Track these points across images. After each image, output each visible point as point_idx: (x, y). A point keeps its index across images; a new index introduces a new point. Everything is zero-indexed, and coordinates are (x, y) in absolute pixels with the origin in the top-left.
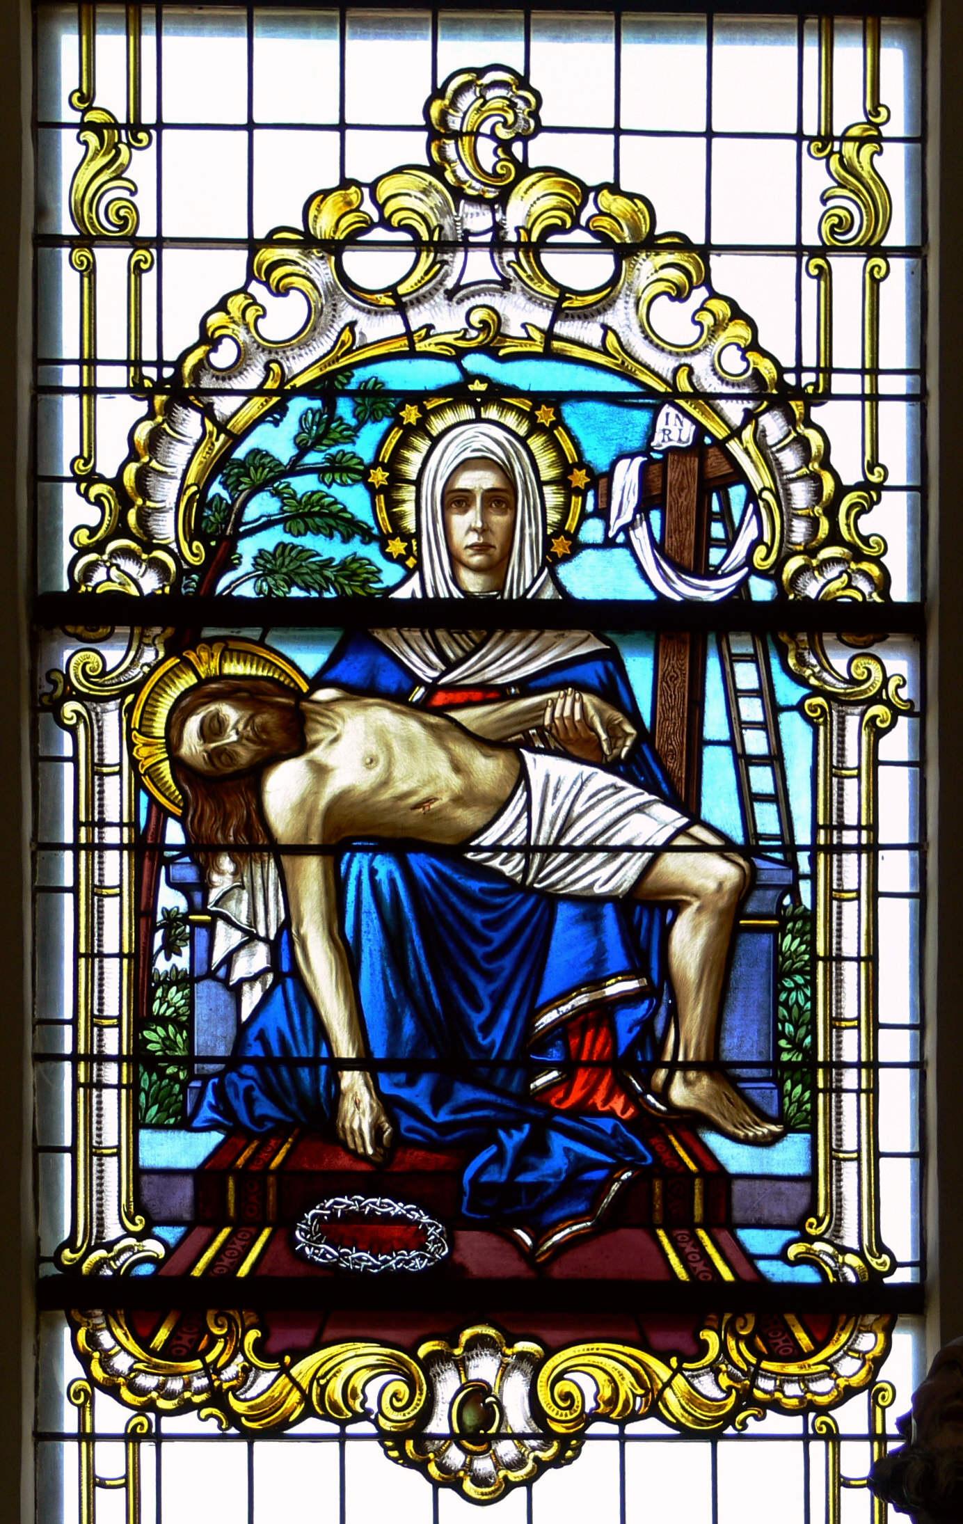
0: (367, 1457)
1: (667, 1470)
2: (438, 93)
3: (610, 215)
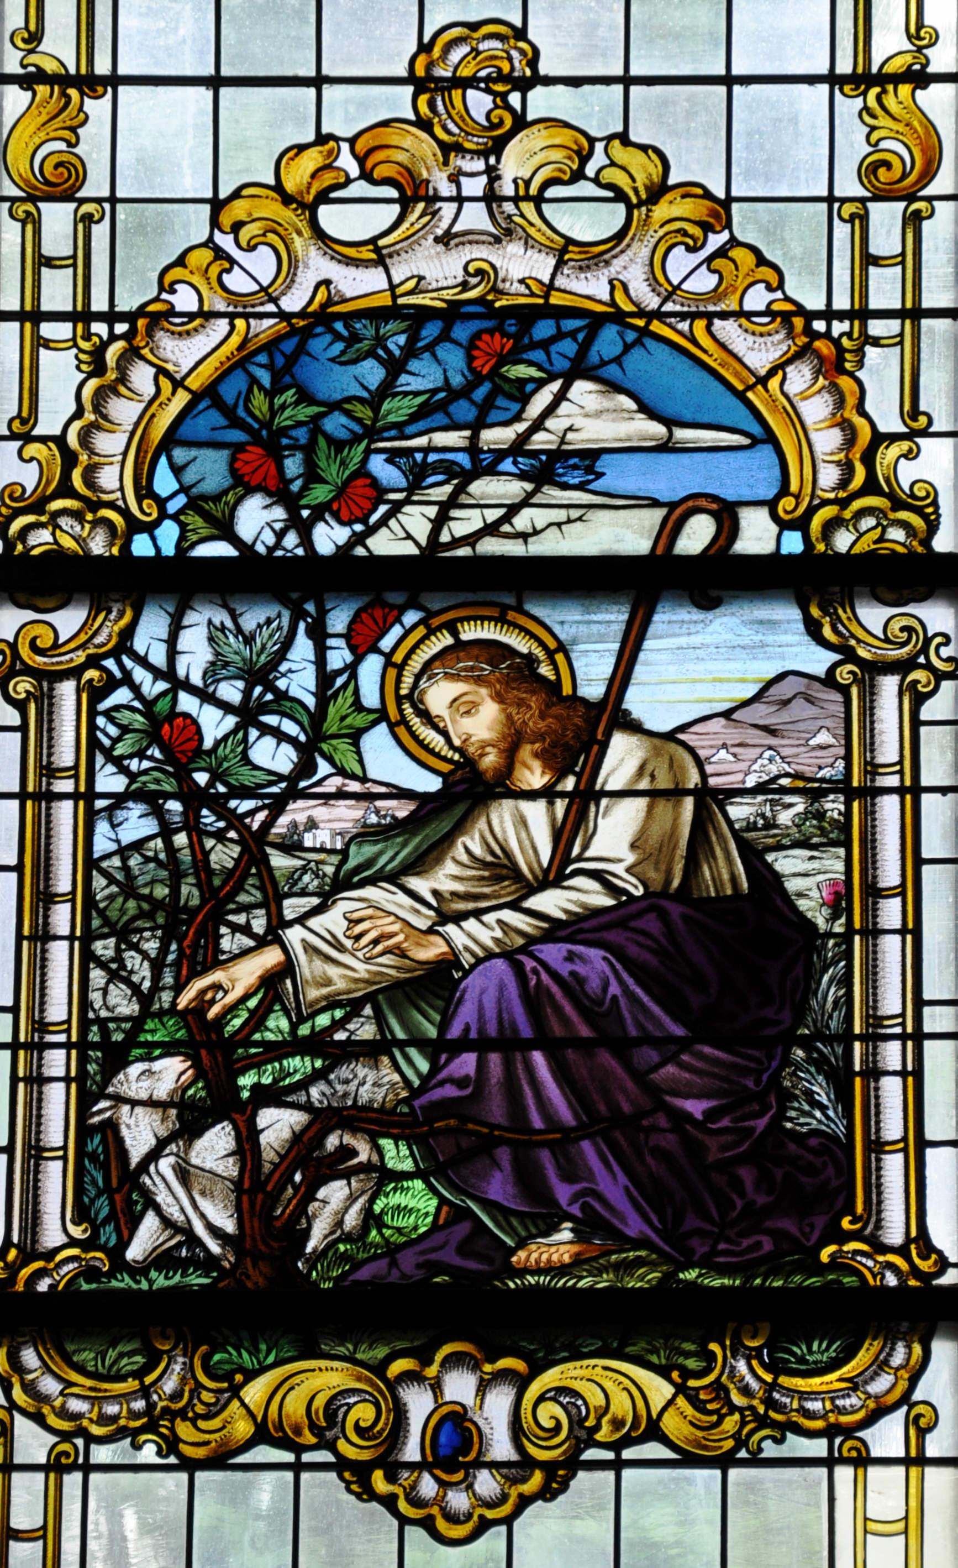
0: (323, 1488)
1: (672, 1505)
2: (424, 48)
3: (623, 168)
